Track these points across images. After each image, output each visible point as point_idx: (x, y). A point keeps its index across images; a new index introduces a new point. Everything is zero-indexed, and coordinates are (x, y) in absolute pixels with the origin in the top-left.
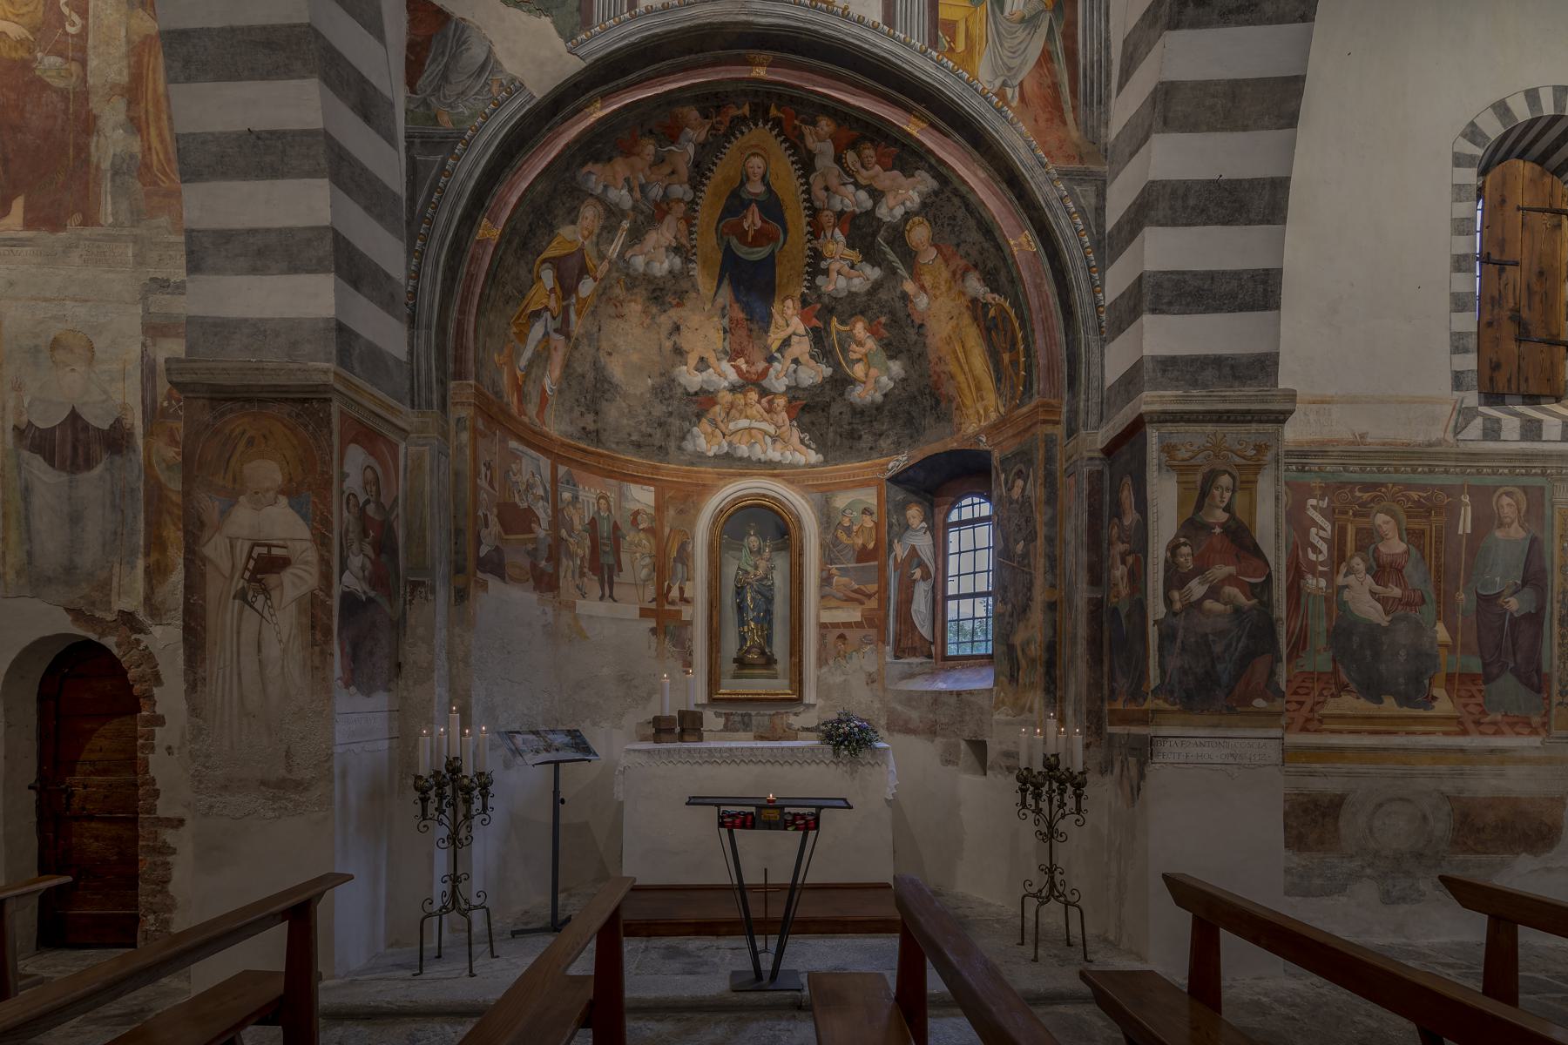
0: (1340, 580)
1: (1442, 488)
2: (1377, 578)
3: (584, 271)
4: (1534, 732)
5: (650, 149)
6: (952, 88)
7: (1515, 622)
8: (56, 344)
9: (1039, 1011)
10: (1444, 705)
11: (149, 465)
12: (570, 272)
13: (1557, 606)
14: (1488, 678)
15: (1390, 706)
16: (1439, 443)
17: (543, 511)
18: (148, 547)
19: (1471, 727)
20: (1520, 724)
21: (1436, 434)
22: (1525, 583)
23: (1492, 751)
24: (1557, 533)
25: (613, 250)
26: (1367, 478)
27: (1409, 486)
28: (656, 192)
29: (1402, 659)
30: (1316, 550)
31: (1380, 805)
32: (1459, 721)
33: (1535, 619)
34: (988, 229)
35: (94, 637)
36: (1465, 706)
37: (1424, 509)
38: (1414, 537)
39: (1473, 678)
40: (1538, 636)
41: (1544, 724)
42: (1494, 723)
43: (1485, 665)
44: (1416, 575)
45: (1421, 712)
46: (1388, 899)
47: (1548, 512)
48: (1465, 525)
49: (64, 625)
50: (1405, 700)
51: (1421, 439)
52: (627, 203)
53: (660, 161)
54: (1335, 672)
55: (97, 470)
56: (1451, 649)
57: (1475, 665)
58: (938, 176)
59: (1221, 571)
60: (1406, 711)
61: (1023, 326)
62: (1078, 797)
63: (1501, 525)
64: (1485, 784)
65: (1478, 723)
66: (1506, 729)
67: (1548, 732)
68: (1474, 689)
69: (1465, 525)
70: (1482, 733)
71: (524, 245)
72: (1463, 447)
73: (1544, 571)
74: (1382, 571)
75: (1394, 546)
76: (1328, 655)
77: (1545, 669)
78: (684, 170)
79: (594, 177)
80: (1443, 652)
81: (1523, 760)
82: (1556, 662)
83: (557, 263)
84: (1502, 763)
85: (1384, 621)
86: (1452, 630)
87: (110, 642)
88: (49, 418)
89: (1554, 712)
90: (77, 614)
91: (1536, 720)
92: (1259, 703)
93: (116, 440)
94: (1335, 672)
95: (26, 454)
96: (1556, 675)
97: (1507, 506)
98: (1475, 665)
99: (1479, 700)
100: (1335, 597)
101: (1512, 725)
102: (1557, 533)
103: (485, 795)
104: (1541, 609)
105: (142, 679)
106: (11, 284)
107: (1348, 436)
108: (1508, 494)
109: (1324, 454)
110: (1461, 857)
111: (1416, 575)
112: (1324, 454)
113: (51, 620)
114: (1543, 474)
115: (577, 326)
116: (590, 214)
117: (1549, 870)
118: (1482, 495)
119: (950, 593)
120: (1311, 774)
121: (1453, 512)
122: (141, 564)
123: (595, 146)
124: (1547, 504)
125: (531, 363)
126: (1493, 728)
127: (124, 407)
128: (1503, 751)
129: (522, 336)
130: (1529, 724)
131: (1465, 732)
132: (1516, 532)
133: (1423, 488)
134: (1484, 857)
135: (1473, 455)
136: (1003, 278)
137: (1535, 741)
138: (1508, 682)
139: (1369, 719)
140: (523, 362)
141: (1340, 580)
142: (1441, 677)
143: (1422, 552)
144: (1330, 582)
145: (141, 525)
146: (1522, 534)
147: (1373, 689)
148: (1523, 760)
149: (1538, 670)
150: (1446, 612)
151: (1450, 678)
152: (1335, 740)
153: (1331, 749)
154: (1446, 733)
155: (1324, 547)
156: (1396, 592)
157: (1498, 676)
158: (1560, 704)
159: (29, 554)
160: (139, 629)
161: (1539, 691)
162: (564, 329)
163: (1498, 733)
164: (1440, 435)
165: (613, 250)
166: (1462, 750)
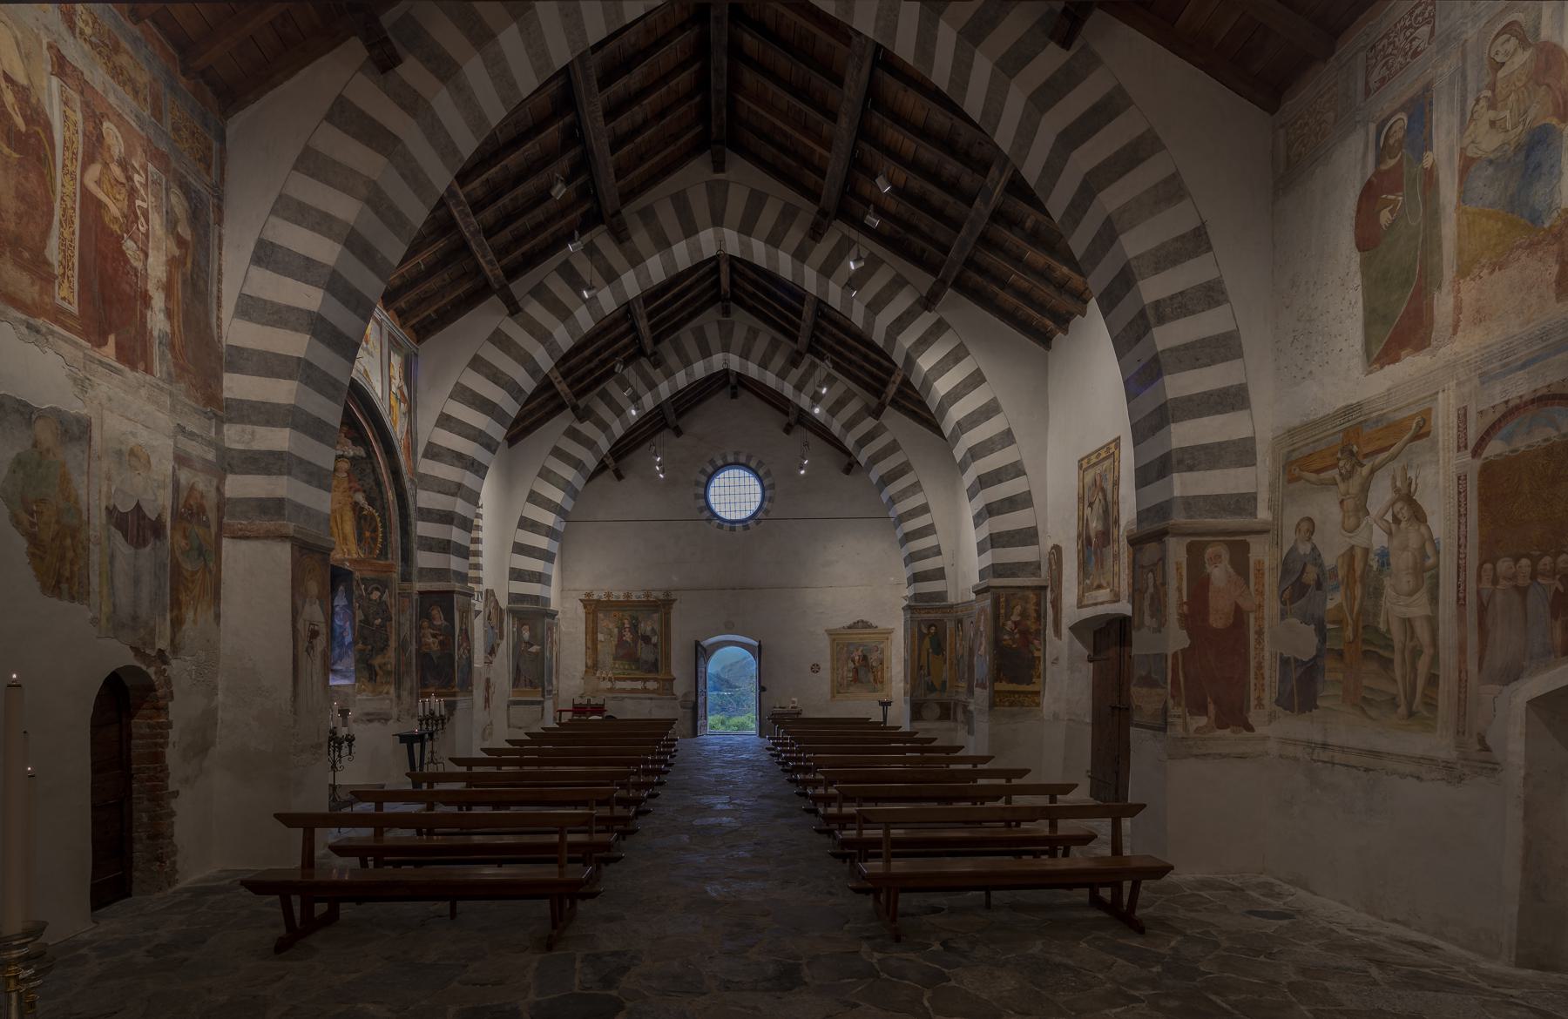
6: (410, 493)
8: (132, 453)
11: (173, 550)
18: (172, 604)
29: (348, 639)
34: (378, 483)
35: (144, 668)
49: (130, 659)
55: (148, 548)
58: (368, 452)
61: (384, 526)
62: (350, 746)
87: (151, 671)
88: (126, 507)
90: (136, 650)
93: (157, 529)
95: (113, 529)
103: (350, 746)
105: (164, 697)
106: (110, 400)
113: (120, 655)
119: (993, 893)
122: (168, 617)
127: (164, 507)
136: (378, 503)
145: (168, 590)
159: (114, 605)
160: (166, 662)
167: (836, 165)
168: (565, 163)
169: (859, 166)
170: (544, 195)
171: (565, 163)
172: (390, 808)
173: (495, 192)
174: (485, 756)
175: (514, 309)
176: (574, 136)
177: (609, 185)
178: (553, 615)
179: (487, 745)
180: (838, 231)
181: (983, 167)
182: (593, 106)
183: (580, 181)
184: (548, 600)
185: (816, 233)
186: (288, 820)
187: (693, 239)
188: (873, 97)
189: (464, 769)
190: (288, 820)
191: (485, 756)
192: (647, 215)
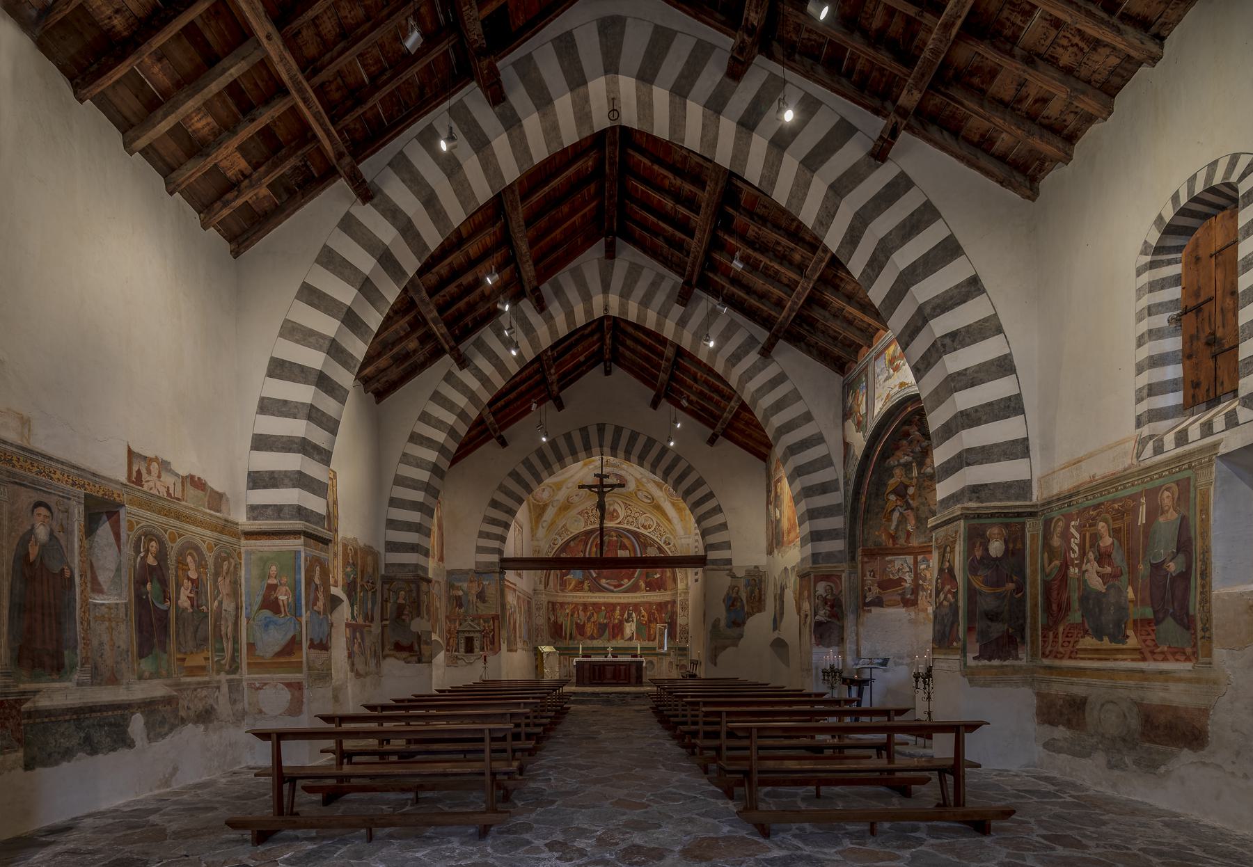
0: (1084, 568)
1: (1130, 497)
2: (1100, 564)
3: (906, 487)
4: (1188, 659)
5: (904, 442)
7: (1173, 580)
9: (510, 575)
10: (1132, 642)
12: (901, 492)
13: (1199, 564)
14: (1158, 621)
15: (1106, 643)
16: (1129, 467)
17: (908, 578)
19: (1148, 655)
20: (1177, 653)
21: (1128, 461)
22: (1178, 550)
23: (1161, 672)
24: (1198, 509)
25: (915, 473)
26: (1096, 502)
27: (1114, 501)
28: (918, 449)
30: (1074, 552)
31: (1102, 705)
32: (1140, 651)
33: (1185, 576)
36: (1145, 641)
37: (1120, 514)
38: (1115, 533)
39: (1149, 622)
40: (1187, 589)
41: (1194, 653)
42: (1162, 653)
43: (1155, 612)
44: (1118, 557)
45: (1120, 646)
46: (1111, 766)
47: (1192, 495)
48: (1142, 519)
50: (1113, 639)
51: (1120, 468)
52: (910, 459)
53: (911, 442)
54: (1083, 623)
56: (1134, 602)
57: (1149, 613)
59: (948, 587)
60: (1114, 646)
63: (1163, 513)
64: (1156, 695)
65: (1153, 653)
66: (1169, 657)
67: (1197, 659)
68: (1149, 629)
69: (1142, 519)
70: (1155, 660)
71: (877, 495)
72: (1143, 465)
73: (1190, 539)
74: (1103, 557)
75: (1107, 541)
76: (1079, 613)
77: (1191, 612)
78: (922, 438)
79: (892, 462)
80: (1131, 605)
81: (1180, 680)
82: (1198, 606)
83: (894, 492)
84: (1167, 681)
85: (1103, 589)
86: (1135, 591)
89: (1199, 643)
91: (1189, 650)
92: (1089, 642)
94: (1083, 623)
96: (1198, 616)
97: (1166, 498)
98: (1149, 613)
99: (1153, 637)
100: (1082, 580)
101: (1174, 654)
102: (1198, 509)
104: (1189, 568)
107: (1088, 479)
108: (1167, 489)
109: (1078, 493)
110: (1147, 745)
111: (1118, 557)
112: (1078, 493)
114: (1190, 468)
115: (914, 503)
116: (897, 471)
117: (1204, 764)
118: (1152, 494)
120: (1072, 684)
121: (1135, 511)
123: (885, 455)
124: (1192, 489)
125: (897, 526)
126: (1162, 656)
128: (1167, 672)
129: (890, 520)
130: (1184, 653)
131: (1144, 659)
132: (1172, 516)
133: (1120, 500)
134: (1160, 747)
135: (1149, 469)
137: (1188, 666)
138: (1169, 623)
139: (1097, 651)
140: (893, 527)
141: (1084, 568)
142: (1130, 624)
143: (1120, 541)
144: (1080, 569)
146: (1176, 515)
147: (1099, 635)
148: (1180, 680)
149: (1187, 614)
150: (1132, 582)
151: (1135, 622)
152: (1082, 664)
153: (1080, 669)
154: (1133, 660)
155: (1076, 549)
156: (1108, 569)
157: (1164, 619)
158: (1203, 638)
161: (1188, 629)
162: (909, 507)
163: (1165, 659)
164: (1129, 462)
165: (915, 473)
166: (1142, 671)
167: (696, 245)
168: (498, 257)
169: (716, 244)
170: (479, 282)
171: (498, 257)
172: (347, 726)
173: (443, 282)
174: (368, 712)
175: (366, 193)
176: (505, 240)
177: (528, 270)
178: (429, 581)
179: (329, 710)
180: (761, 70)
181: (729, 399)
182: (518, 215)
183: (508, 270)
184: (426, 570)
185: (736, 71)
186: (263, 735)
187: (581, 90)
188: (676, 364)
189: (331, 726)
190: (263, 735)
191: (368, 712)
192: (527, 70)
